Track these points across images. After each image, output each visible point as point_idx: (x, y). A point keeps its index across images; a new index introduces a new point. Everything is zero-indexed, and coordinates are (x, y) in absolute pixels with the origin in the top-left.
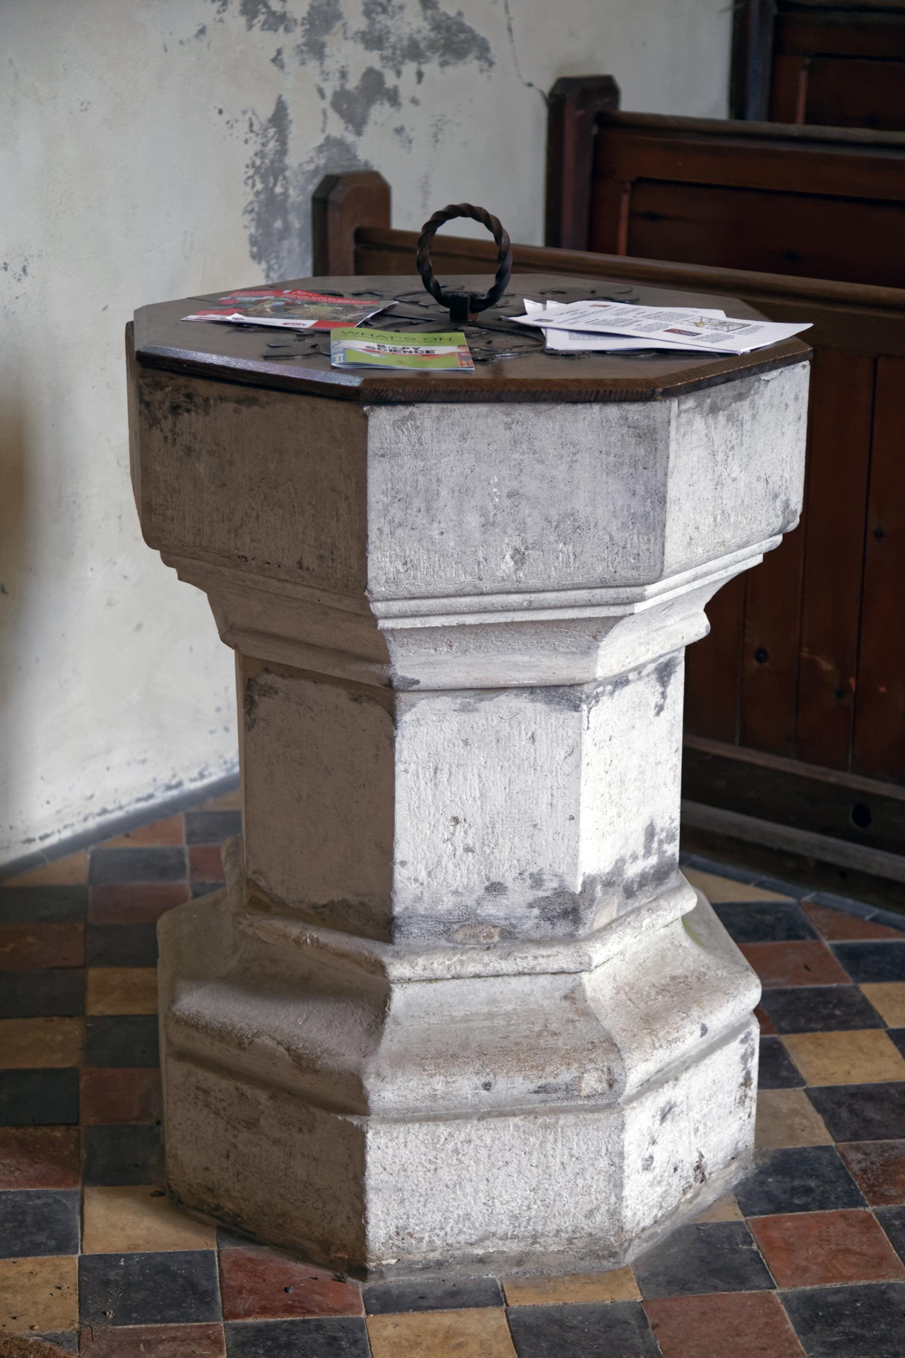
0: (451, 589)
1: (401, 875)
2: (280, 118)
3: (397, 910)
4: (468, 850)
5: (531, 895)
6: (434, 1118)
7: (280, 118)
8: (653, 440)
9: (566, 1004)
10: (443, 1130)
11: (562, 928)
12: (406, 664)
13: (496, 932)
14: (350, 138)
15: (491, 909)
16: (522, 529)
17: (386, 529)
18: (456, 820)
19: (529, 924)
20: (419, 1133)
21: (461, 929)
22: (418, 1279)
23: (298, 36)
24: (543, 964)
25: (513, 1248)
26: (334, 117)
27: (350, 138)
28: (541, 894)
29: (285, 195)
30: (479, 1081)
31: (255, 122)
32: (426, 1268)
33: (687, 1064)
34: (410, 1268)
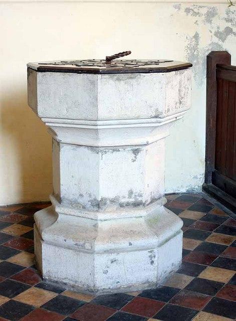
0: (54, 117)
1: (62, 188)
2: (196, 37)
3: (61, 196)
4: (75, 184)
5: (89, 199)
6: (56, 245)
7: (196, 37)
8: (94, 83)
9: (93, 227)
10: (57, 249)
11: (96, 209)
12: (61, 137)
13: (81, 206)
14: (220, 43)
15: (80, 200)
16: (67, 104)
17: (41, 101)
18: (73, 177)
19: (88, 206)
20: (53, 248)
21: (74, 204)
22: (52, 284)
23: (203, 17)
24: (87, 216)
25: (72, 283)
26: (214, 36)
27: (220, 43)
28: (91, 199)
29: (198, 55)
30: (64, 239)
31: (188, 37)
32: (54, 282)
33: (123, 250)
34: (50, 280)
